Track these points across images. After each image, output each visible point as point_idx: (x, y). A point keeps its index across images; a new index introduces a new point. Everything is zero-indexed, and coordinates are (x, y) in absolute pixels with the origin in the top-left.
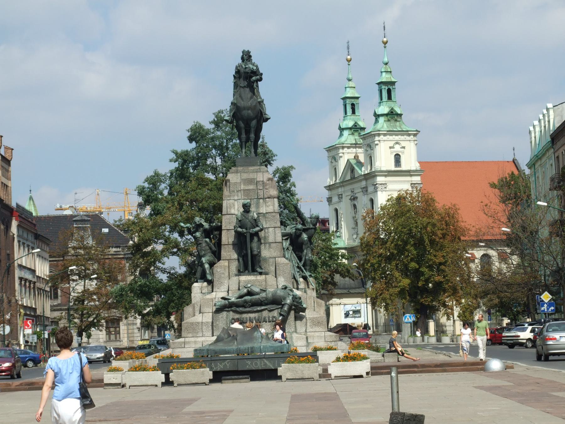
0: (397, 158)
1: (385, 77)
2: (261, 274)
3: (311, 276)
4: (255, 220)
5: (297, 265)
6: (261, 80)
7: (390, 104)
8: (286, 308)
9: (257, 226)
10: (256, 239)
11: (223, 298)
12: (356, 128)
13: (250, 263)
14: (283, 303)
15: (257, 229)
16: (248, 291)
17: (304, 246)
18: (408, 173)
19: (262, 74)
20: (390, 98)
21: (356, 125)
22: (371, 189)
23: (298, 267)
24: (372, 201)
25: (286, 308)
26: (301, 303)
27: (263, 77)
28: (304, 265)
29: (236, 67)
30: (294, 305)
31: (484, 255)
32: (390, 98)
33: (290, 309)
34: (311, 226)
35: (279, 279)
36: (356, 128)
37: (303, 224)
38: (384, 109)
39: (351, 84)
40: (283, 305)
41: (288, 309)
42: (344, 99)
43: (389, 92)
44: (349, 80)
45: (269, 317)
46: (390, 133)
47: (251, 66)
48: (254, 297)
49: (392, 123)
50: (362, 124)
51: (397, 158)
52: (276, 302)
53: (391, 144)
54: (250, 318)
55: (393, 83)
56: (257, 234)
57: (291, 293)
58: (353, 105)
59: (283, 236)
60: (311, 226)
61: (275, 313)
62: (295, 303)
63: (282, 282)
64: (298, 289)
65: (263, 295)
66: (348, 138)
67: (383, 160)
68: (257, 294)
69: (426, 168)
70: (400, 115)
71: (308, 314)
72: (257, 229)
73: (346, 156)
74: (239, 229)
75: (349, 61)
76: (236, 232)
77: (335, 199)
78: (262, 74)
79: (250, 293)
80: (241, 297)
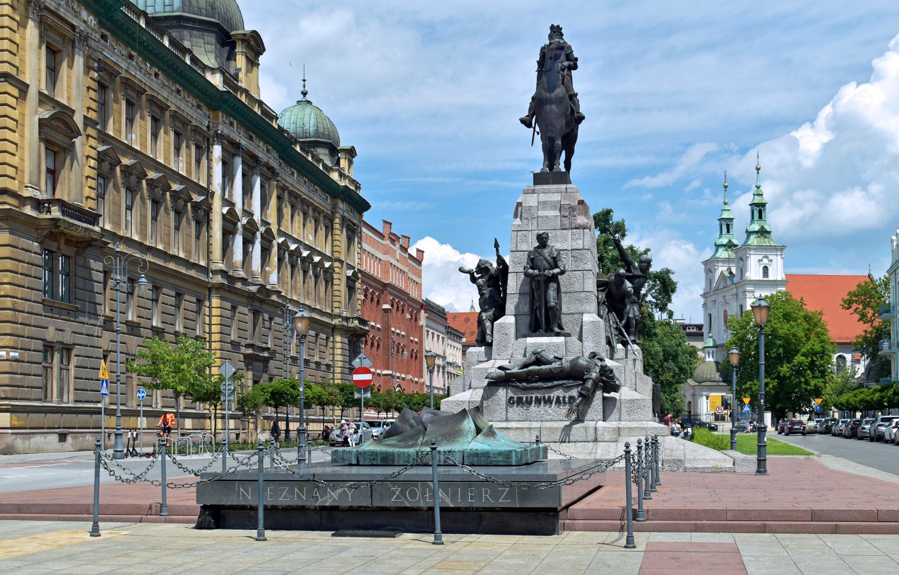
0: (766, 269)
1: (757, 200)
2: (558, 334)
3: (634, 342)
4: (554, 258)
5: (615, 326)
6: (575, 67)
7: (762, 223)
8: (589, 384)
9: (557, 266)
10: (553, 286)
11: (500, 368)
12: (730, 246)
13: (543, 318)
14: (585, 377)
15: (556, 271)
16: (537, 358)
17: (626, 300)
18: (776, 283)
19: (576, 59)
20: (760, 217)
21: (730, 241)
22: (740, 295)
23: (617, 329)
24: (741, 306)
25: (589, 384)
26: (613, 378)
27: (578, 63)
28: (627, 326)
29: (542, 49)
30: (603, 381)
31: (840, 356)
32: (760, 217)
33: (596, 386)
34: (640, 273)
35: (585, 343)
36: (730, 246)
37: (628, 270)
38: (756, 227)
39: (727, 207)
40: (585, 381)
41: (592, 385)
42: (721, 220)
43: (760, 212)
44: (725, 204)
45: (564, 398)
46: (759, 248)
47: (561, 41)
48: (543, 367)
49: (762, 239)
50: (735, 242)
51: (766, 269)
52: (575, 374)
53: (760, 257)
54: (536, 397)
55: (764, 205)
56: (554, 278)
57: (599, 363)
58: (728, 225)
59: (598, 286)
60: (640, 273)
61: (574, 393)
62: (604, 378)
63: (589, 346)
64: (612, 359)
65: (556, 365)
66: (723, 254)
67: (754, 272)
68: (550, 363)
69: (790, 279)
70: (769, 233)
71: (625, 394)
72: (556, 271)
73: (722, 269)
74: (531, 271)
75: (726, 187)
76: (526, 274)
77: (709, 305)
78: (576, 59)
79: (539, 361)
80: (526, 366)
